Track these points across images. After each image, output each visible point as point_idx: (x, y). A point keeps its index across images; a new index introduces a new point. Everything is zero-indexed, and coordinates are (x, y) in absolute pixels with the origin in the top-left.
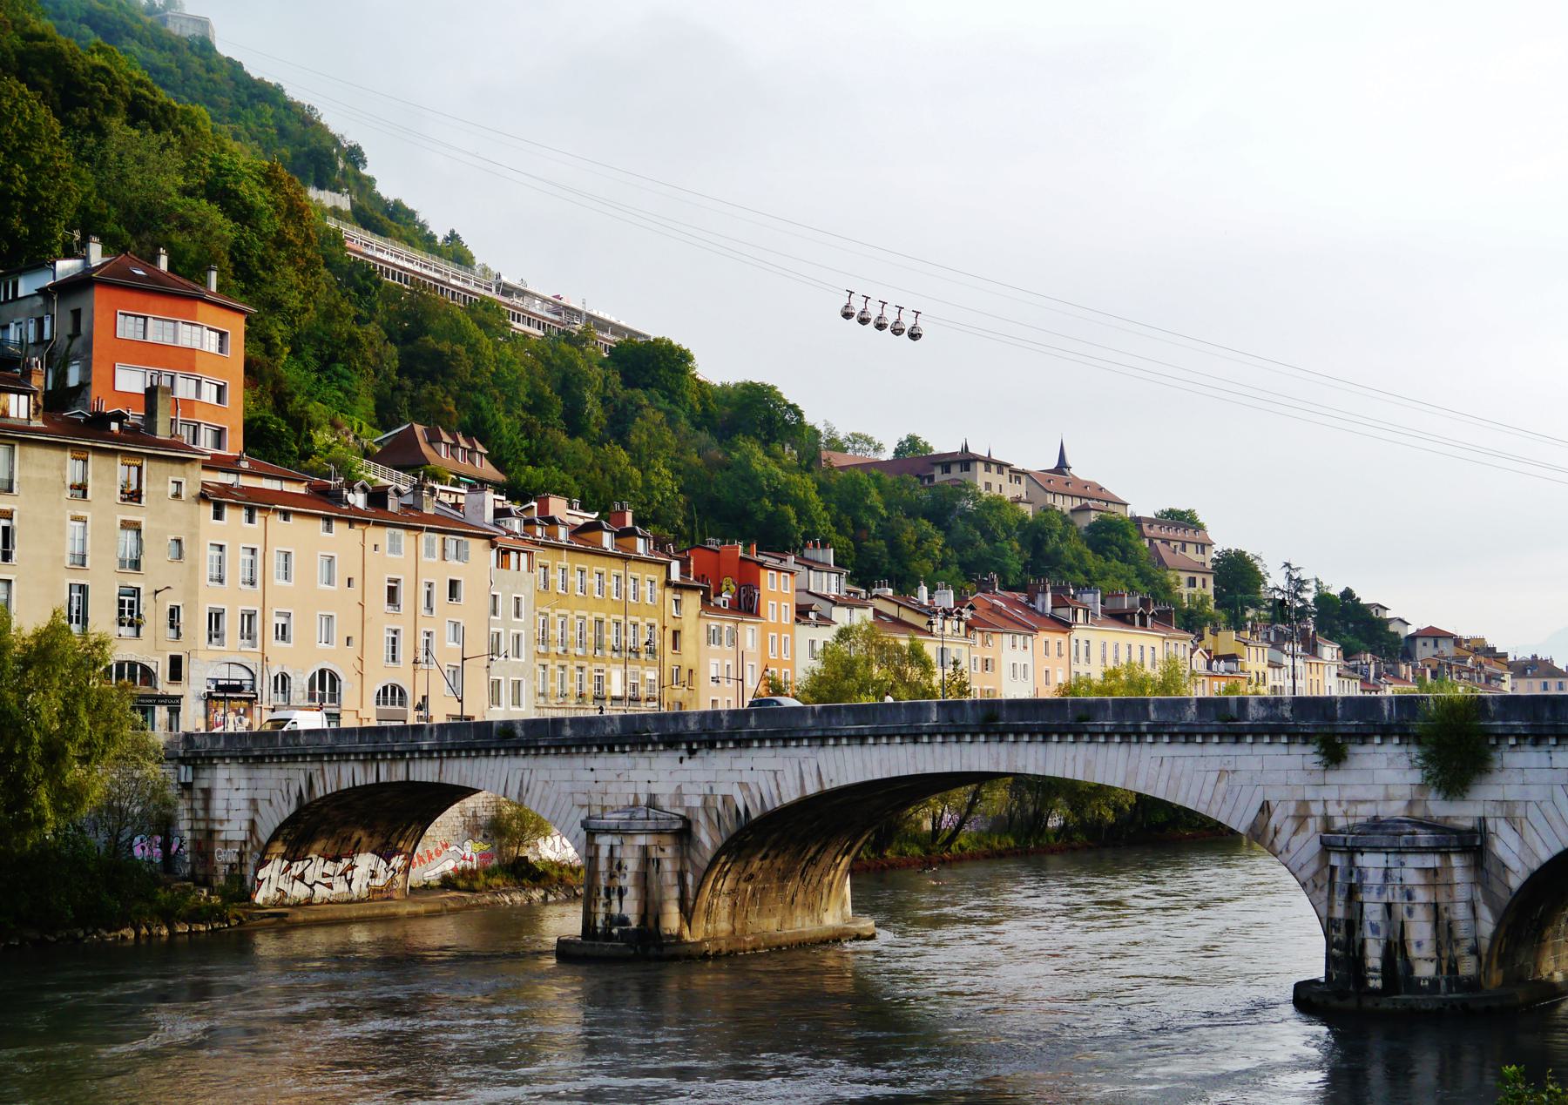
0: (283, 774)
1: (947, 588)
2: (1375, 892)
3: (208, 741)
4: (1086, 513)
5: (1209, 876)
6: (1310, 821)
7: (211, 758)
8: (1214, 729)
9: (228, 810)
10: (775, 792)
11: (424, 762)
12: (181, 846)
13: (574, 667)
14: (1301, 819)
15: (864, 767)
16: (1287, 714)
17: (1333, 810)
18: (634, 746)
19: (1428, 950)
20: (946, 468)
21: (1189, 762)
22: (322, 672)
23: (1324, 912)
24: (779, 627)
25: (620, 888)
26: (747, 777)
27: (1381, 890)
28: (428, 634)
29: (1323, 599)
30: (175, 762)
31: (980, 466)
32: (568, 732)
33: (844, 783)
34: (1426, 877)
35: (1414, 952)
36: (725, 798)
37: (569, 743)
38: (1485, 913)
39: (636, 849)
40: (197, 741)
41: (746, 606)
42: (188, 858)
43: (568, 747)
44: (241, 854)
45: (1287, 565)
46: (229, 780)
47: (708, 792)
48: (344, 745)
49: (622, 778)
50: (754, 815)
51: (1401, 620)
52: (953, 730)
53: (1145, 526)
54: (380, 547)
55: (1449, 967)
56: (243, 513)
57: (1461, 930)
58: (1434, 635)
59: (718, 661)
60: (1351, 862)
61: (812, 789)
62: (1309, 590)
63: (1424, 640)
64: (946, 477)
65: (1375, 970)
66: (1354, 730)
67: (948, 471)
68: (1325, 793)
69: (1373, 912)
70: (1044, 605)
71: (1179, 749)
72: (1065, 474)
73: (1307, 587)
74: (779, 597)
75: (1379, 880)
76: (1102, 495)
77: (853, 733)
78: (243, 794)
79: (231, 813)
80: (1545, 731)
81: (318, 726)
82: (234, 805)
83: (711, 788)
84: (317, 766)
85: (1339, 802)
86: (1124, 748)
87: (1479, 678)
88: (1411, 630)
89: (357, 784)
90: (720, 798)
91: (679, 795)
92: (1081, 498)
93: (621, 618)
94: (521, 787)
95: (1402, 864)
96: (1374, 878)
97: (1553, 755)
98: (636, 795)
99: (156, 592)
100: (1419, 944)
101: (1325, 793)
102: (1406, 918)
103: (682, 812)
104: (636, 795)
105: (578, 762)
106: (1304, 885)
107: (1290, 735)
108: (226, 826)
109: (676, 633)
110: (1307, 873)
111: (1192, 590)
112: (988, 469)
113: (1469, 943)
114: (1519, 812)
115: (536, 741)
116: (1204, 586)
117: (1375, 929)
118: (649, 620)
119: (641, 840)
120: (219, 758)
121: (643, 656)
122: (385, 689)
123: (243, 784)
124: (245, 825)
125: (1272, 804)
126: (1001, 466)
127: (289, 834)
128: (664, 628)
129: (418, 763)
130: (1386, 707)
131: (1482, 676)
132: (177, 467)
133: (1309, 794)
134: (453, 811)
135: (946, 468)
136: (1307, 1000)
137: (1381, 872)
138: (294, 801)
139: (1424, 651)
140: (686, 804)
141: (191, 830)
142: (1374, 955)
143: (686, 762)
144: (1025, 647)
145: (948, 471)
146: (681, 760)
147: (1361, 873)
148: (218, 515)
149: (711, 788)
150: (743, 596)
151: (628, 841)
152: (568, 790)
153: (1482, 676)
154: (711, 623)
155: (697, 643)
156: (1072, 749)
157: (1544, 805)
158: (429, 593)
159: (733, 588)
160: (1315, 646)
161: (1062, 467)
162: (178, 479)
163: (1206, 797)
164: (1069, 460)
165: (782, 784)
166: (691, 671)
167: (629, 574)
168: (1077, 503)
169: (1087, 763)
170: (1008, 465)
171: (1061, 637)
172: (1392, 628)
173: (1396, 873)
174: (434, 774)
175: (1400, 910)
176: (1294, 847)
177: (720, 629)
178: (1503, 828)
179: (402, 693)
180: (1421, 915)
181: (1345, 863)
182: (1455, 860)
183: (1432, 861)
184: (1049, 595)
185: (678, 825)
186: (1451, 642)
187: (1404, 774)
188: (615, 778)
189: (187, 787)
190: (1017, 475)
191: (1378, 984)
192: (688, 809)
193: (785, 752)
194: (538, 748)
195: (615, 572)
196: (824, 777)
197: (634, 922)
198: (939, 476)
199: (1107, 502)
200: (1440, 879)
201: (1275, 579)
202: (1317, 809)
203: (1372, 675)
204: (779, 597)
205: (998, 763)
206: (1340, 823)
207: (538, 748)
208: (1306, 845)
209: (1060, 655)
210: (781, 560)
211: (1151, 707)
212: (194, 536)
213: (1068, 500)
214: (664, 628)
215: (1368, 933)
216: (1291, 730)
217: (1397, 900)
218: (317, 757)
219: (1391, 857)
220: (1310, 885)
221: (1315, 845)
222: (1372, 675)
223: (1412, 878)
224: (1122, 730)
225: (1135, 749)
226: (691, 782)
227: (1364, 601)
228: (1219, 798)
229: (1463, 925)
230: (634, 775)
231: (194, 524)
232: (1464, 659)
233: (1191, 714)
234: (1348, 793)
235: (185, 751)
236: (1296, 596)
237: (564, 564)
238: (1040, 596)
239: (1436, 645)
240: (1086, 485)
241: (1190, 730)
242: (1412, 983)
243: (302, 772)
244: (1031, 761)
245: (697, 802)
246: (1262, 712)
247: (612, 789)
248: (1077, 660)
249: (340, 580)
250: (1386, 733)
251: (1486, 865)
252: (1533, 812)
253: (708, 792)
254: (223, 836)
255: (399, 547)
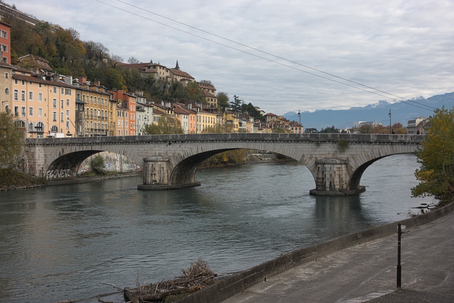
0: (55, 148)
1: (169, 102)
2: (328, 172)
3: (34, 140)
4: (184, 81)
5: (291, 169)
6: (313, 158)
7: (35, 145)
8: (293, 140)
9: (39, 157)
10: (191, 152)
11: (97, 146)
12: (26, 166)
13: (90, 122)
14: (311, 158)
15: (213, 147)
16: (309, 137)
17: (317, 156)
18: (155, 142)
19: (338, 183)
20: (149, 67)
21: (287, 147)
22: (39, 123)
23: (316, 176)
24: (133, 112)
25: (155, 174)
26: (184, 149)
27: (329, 172)
28: (55, 113)
29: (244, 105)
30: (25, 145)
31: (158, 67)
32: (137, 139)
33: (208, 150)
34: (338, 169)
35: (335, 184)
36: (178, 154)
37: (138, 141)
38: (348, 176)
39: (158, 165)
40: (30, 141)
41: (125, 106)
42: (28, 169)
43: (138, 142)
44: (42, 168)
45: (235, 96)
46: (39, 150)
47: (174, 152)
48: (73, 141)
49: (151, 149)
50: (186, 158)
51: (263, 111)
52: (235, 139)
53: (199, 85)
54: (52, 91)
55: (342, 186)
56: (39, 85)
57: (344, 179)
58: (271, 115)
59: (120, 120)
60: (323, 166)
61: (200, 152)
62: (241, 103)
63: (269, 117)
64: (149, 70)
65: (328, 187)
66: (323, 140)
67: (149, 68)
68: (316, 153)
69: (328, 176)
70: (190, 107)
71: (285, 144)
72: (178, 70)
73: (240, 102)
74: (133, 104)
75: (329, 170)
76: (188, 76)
77: (211, 140)
78: (43, 153)
79: (40, 158)
80: (361, 141)
81: (63, 137)
82: (41, 156)
83: (175, 152)
84: (65, 146)
85: (319, 155)
86: (273, 144)
87: (284, 127)
88: (265, 114)
89: (77, 151)
90: (177, 154)
91: (167, 153)
92: (183, 76)
93: (100, 109)
94: (124, 151)
95: (334, 167)
96: (328, 169)
97: (362, 146)
98: (155, 153)
99: (3, 102)
100: (336, 182)
101: (316, 153)
102: (334, 177)
103: (167, 157)
104: (155, 153)
105: (140, 146)
106: (311, 171)
107: (309, 141)
108: (38, 161)
109: (111, 113)
110: (312, 169)
111: (212, 102)
112: (160, 68)
113: (345, 182)
114: (355, 157)
115: (129, 141)
116: (215, 101)
117: (328, 179)
118: (105, 110)
119: (159, 163)
120: (37, 145)
121: (104, 119)
122: (53, 127)
123: (43, 151)
124: (43, 161)
125: (305, 155)
126: (164, 67)
127: (55, 163)
128: (109, 112)
129: (95, 146)
130: (329, 136)
131: (285, 126)
132: (7, 70)
133: (313, 153)
134: (89, 158)
135: (149, 67)
136: (312, 193)
137: (329, 168)
138: (58, 155)
139: (268, 119)
140: (168, 155)
141: (28, 162)
142: (328, 185)
143: (168, 146)
144: (187, 118)
145: (149, 68)
146: (167, 145)
147: (325, 168)
148: (16, 83)
149: (175, 152)
150: (124, 104)
151: (156, 163)
152: (137, 152)
153: (285, 126)
154: (119, 111)
155: (116, 116)
156: (261, 144)
157: (360, 155)
158: (62, 103)
159: (121, 101)
160: (249, 118)
161: (177, 67)
162: (7, 73)
163: (291, 153)
164: (179, 66)
165: (193, 151)
166: (114, 123)
167: (102, 98)
168: (182, 78)
169: (264, 147)
170: (165, 67)
171: (195, 116)
172: (261, 113)
173: (332, 168)
174: (99, 149)
175: (333, 176)
176: (309, 163)
177: (120, 112)
178: (352, 160)
179: (57, 128)
180: (337, 176)
181: (322, 166)
182: (343, 166)
183: (339, 166)
184: (191, 104)
185: (167, 160)
186: (275, 117)
187: (332, 149)
188: (150, 149)
189: (27, 151)
190: (167, 70)
191: (329, 190)
192: (169, 156)
193: (194, 144)
194: (129, 142)
195: (99, 97)
196: (203, 149)
197: (158, 181)
198: (147, 70)
199: (189, 78)
200: (341, 170)
201: (231, 99)
202: (314, 156)
203: (260, 126)
204: (133, 104)
205: (244, 147)
206: (319, 159)
207: (129, 142)
208: (312, 163)
209: (194, 120)
210: (131, 94)
211: (279, 135)
212: (11, 88)
213: (180, 77)
214: (109, 112)
215: (327, 180)
216: (309, 140)
217: (333, 173)
218: (66, 144)
219: (331, 165)
220: (312, 171)
221: (314, 162)
222: (260, 126)
223: (335, 169)
224: (273, 140)
225: (275, 144)
226: (170, 150)
227: (254, 106)
228: (293, 154)
229: (344, 178)
230: (154, 149)
231: (11, 85)
232: (279, 122)
233: (288, 137)
234: (321, 153)
235: (27, 143)
236: (237, 104)
237: (88, 95)
238: (189, 104)
239: (272, 118)
240: (185, 73)
241: (288, 140)
242: (335, 190)
243: (60, 148)
244: (252, 146)
245: (171, 155)
246: (303, 137)
247: (149, 152)
248: (198, 121)
249: (43, 99)
250: (329, 141)
251: (348, 167)
252: (358, 157)
253: (174, 152)
254: (38, 164)
255: (56, 91)
